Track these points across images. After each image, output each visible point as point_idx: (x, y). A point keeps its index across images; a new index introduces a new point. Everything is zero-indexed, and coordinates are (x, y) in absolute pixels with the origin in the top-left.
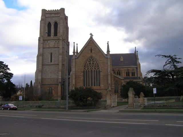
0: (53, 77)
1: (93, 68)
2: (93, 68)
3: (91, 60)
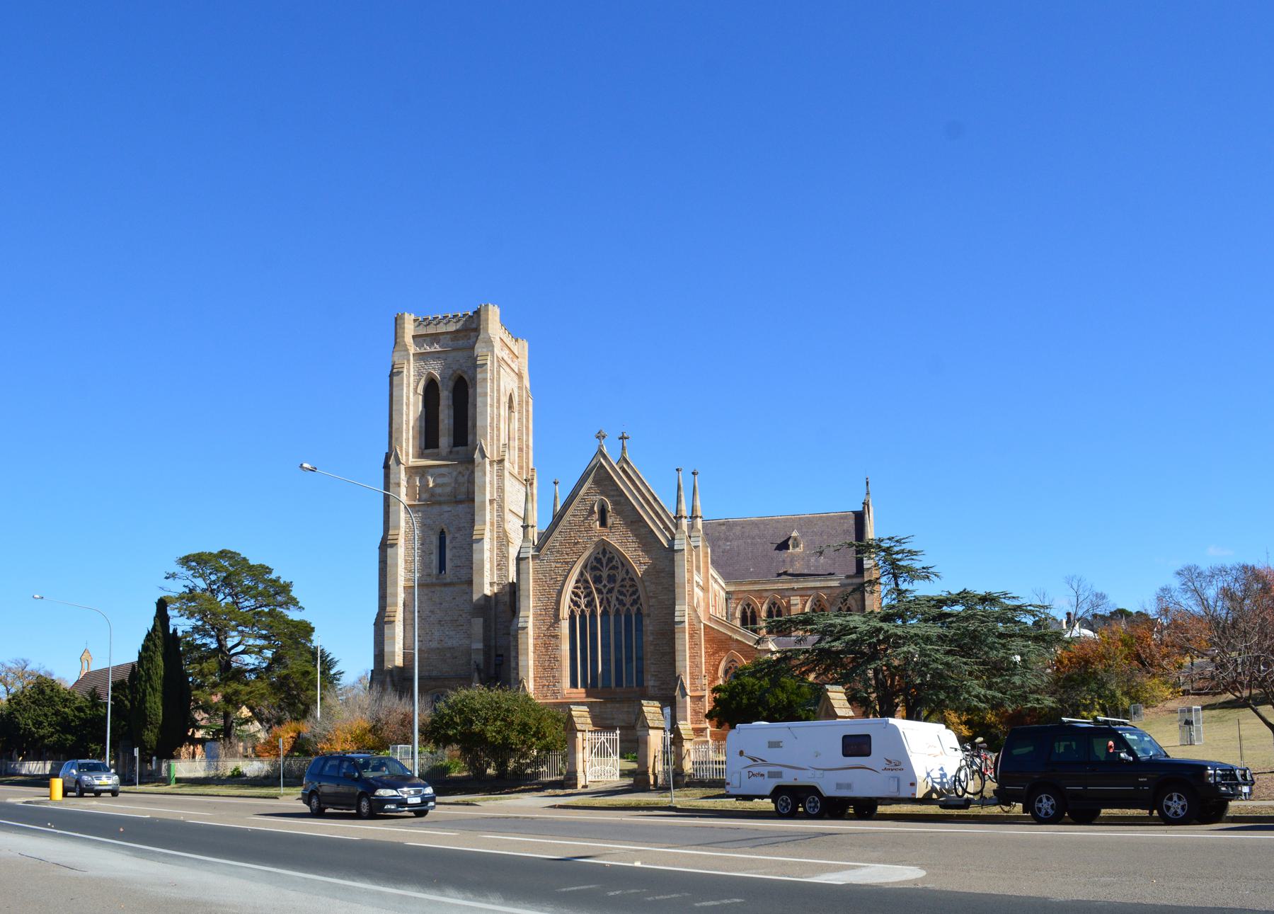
0: (450, 643)
1: (614, 601)
2: (614, 601)
3: (602, 564)
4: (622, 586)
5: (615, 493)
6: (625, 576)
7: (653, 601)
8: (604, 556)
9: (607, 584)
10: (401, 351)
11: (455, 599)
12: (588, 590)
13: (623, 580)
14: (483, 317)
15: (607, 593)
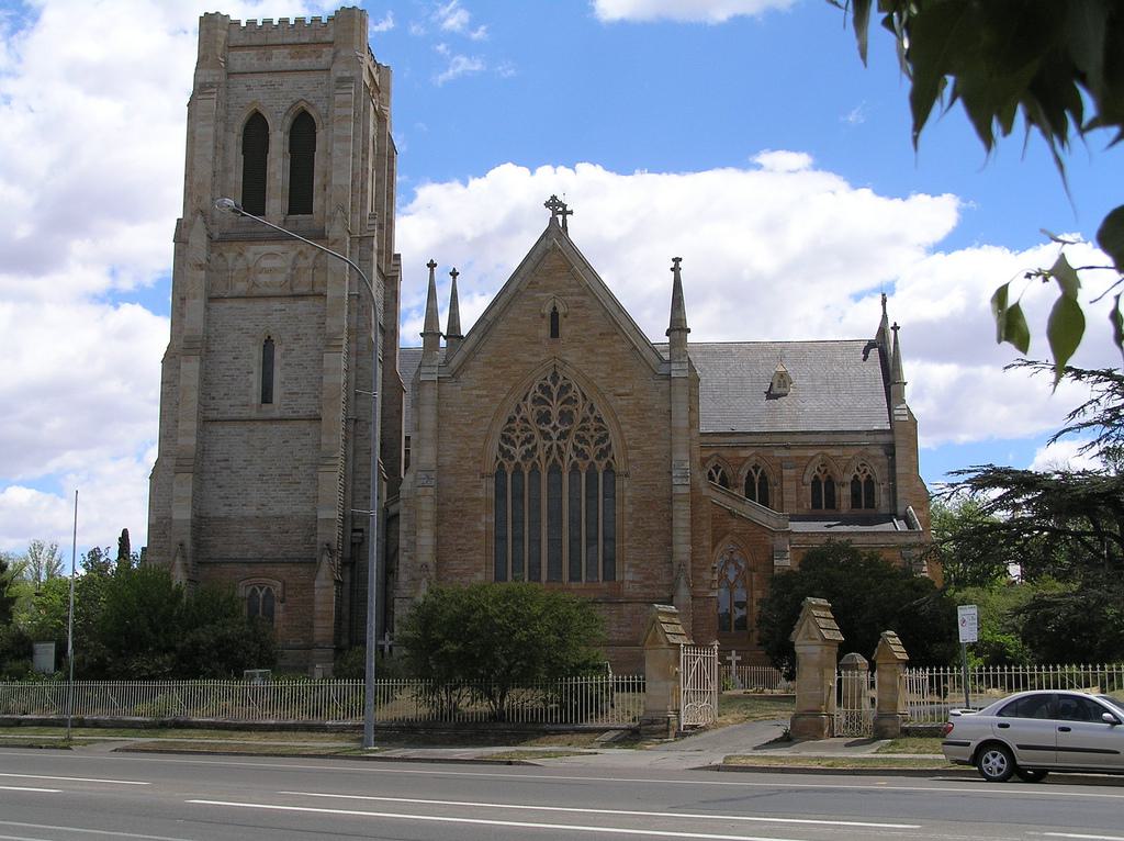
0: (276, 510)
1: (569, 451)
2: (569, 451)
3: (550, 395)
4: (583, 429)
5: (576, 290)
6: (588, 413)
7: (633, 454)
8: (555, 384)
12: (528, 434)
13: (585, 420)
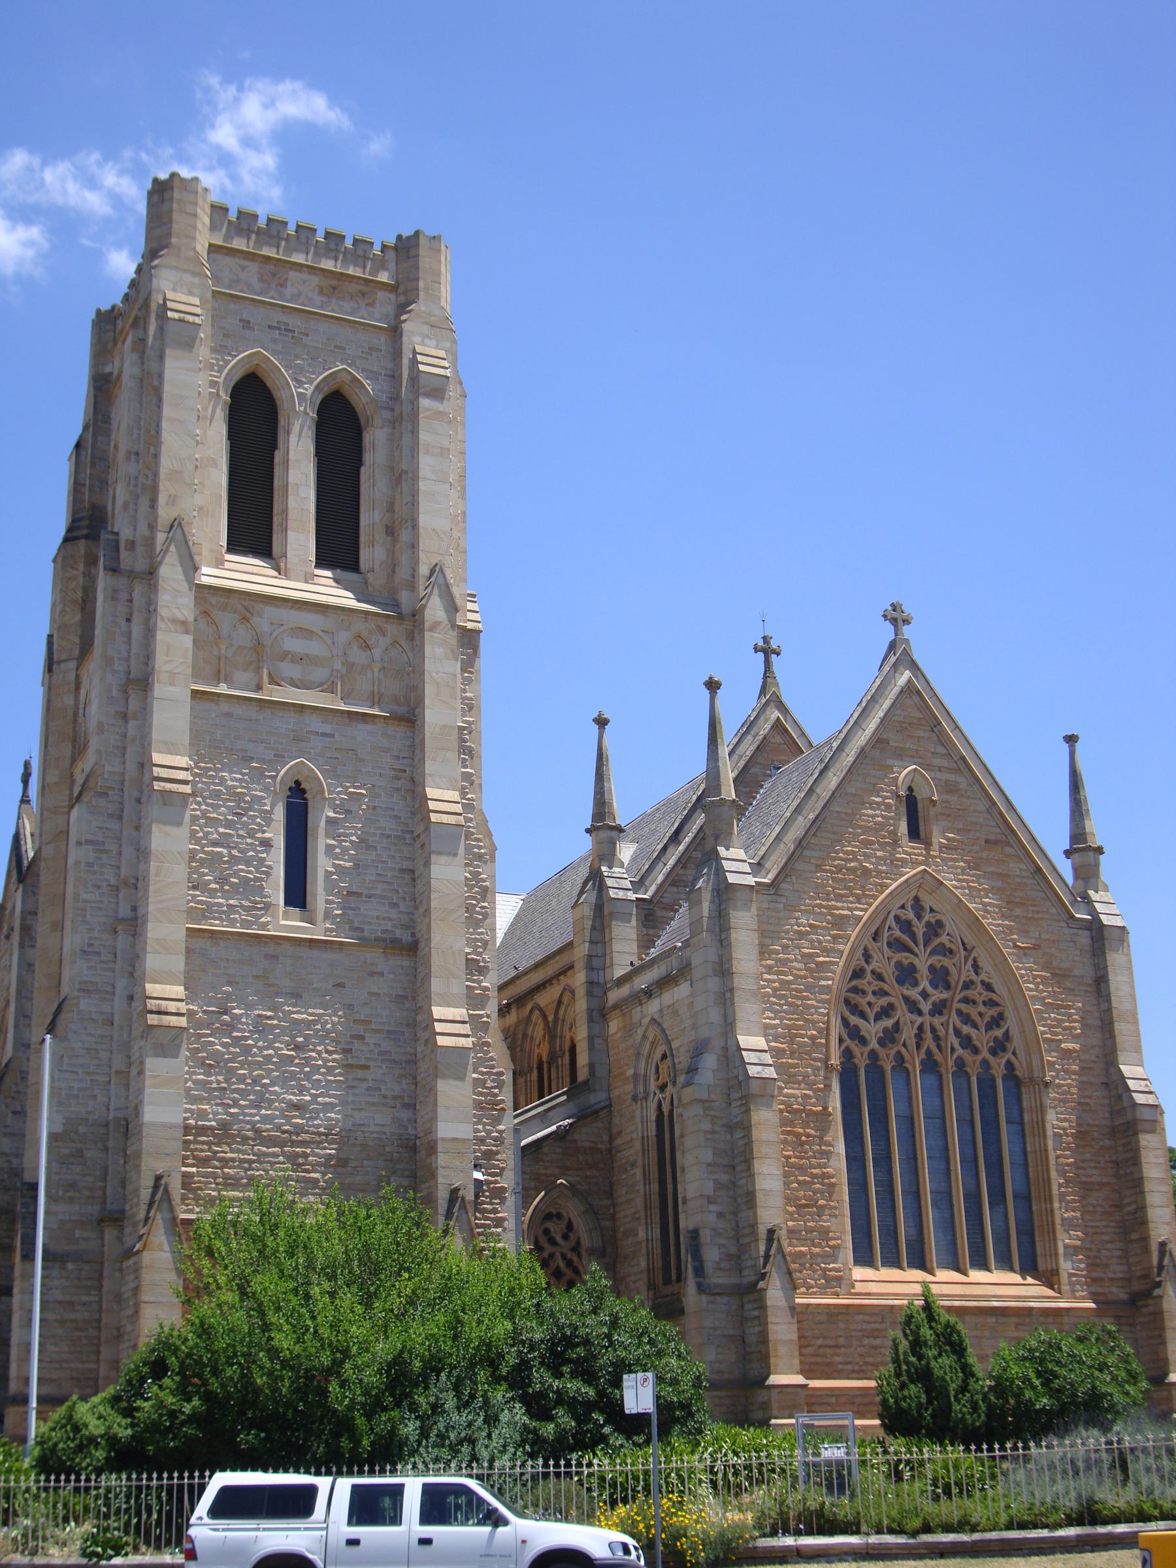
5: (945, 763)
6: (983, 976)
9: (930, 990)
10: (186, 271)
11: (341, 985)
14: (425, 261)
15: (932, 1013)
